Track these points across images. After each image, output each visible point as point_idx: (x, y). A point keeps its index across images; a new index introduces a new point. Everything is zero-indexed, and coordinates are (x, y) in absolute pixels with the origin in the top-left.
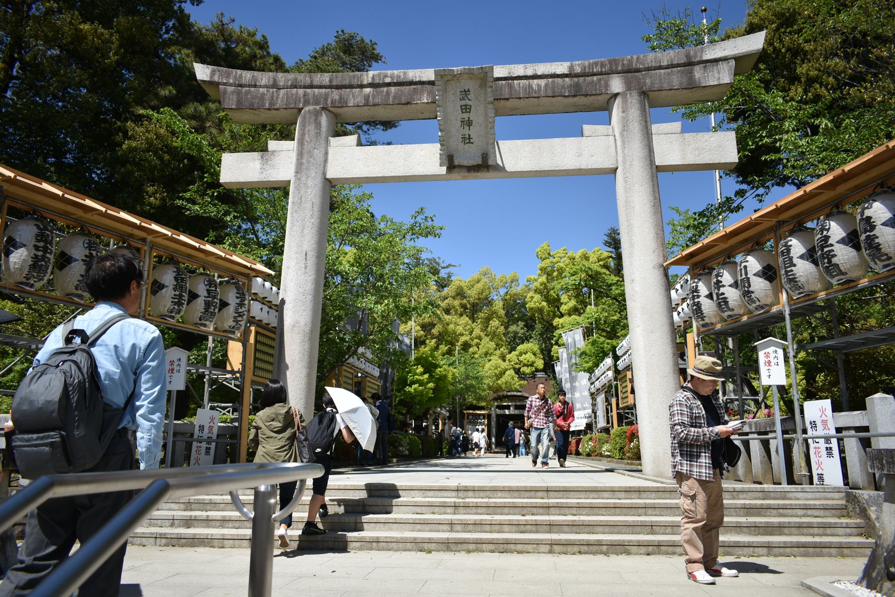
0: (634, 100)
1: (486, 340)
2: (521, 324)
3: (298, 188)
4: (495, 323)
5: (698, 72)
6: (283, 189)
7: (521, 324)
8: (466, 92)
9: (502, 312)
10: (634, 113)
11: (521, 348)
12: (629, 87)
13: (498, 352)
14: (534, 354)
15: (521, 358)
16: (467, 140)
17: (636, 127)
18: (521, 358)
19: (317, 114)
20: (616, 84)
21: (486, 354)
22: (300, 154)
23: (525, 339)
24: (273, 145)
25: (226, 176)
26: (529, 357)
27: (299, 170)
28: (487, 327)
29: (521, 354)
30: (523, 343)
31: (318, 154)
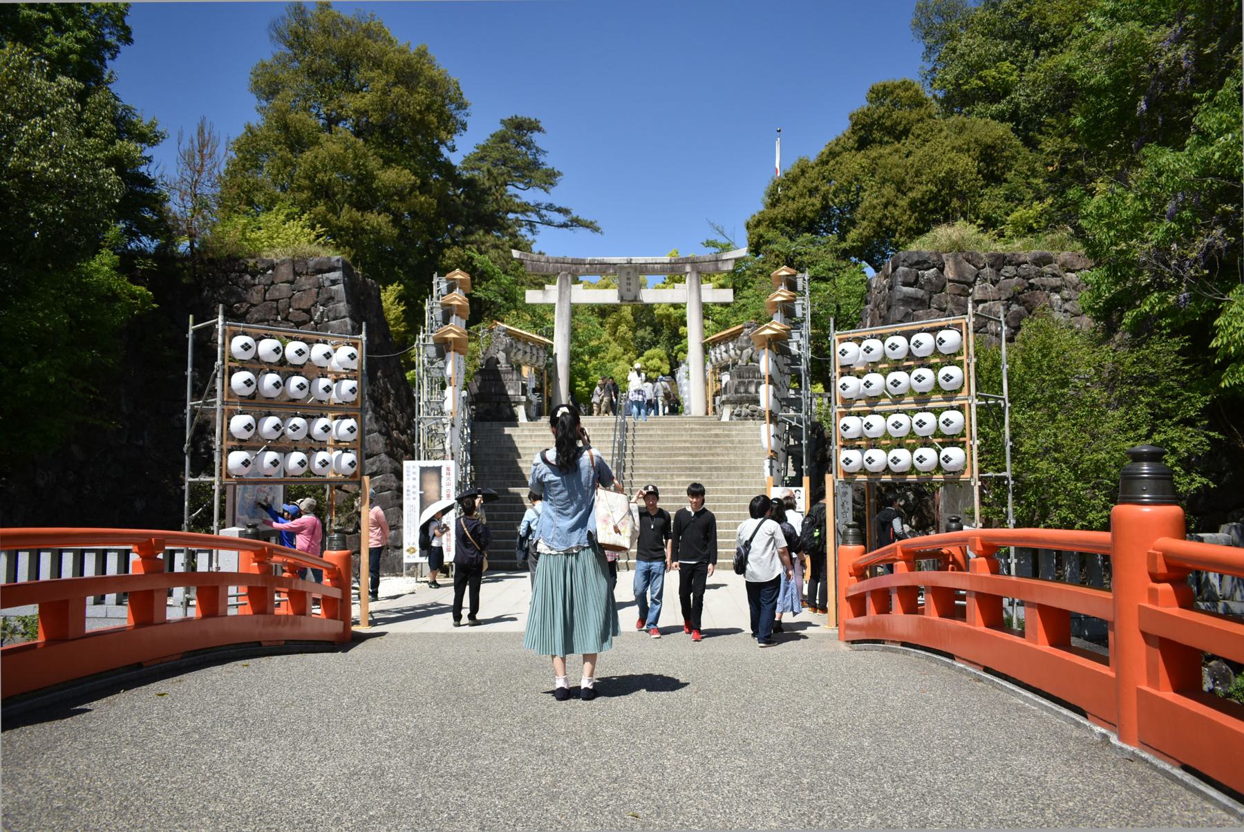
0: (694, 275)
1: (614, 344)
2: (649, 329)
3: (560, 308)
4: (623, 328)
5: (720, 264)
6: (551, 308)
7: (649, 329)
8: (629, 273)
9: (630, 318)
10: (694, 281)
11: (648, 353)
12: (693, 270)
13: (626, 357)
14: (661, 360)
15: (648, 364)
16: (629, 290)
17: (695, 287)
18: (648, 364)
19: (567, 275)
20: (688, 268)
21: (614, 359)
22: (560, 293)
23: (653, 344)
24: (547, 287)
25: (528, 301)
26: (655, 362)
27: (560, 299)
28: (615, 332)
29: (648, 360)
30: (650, 348)
31: (568, 292)
